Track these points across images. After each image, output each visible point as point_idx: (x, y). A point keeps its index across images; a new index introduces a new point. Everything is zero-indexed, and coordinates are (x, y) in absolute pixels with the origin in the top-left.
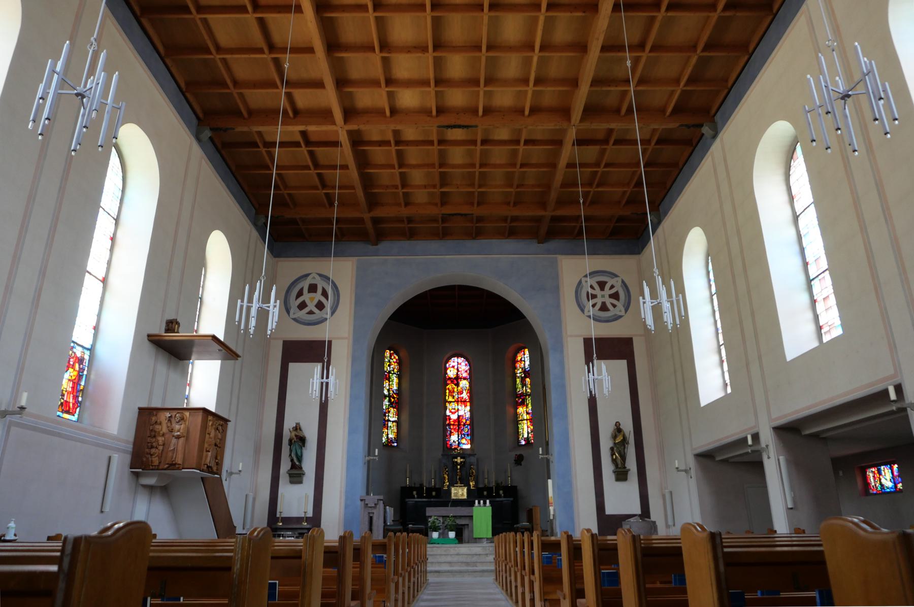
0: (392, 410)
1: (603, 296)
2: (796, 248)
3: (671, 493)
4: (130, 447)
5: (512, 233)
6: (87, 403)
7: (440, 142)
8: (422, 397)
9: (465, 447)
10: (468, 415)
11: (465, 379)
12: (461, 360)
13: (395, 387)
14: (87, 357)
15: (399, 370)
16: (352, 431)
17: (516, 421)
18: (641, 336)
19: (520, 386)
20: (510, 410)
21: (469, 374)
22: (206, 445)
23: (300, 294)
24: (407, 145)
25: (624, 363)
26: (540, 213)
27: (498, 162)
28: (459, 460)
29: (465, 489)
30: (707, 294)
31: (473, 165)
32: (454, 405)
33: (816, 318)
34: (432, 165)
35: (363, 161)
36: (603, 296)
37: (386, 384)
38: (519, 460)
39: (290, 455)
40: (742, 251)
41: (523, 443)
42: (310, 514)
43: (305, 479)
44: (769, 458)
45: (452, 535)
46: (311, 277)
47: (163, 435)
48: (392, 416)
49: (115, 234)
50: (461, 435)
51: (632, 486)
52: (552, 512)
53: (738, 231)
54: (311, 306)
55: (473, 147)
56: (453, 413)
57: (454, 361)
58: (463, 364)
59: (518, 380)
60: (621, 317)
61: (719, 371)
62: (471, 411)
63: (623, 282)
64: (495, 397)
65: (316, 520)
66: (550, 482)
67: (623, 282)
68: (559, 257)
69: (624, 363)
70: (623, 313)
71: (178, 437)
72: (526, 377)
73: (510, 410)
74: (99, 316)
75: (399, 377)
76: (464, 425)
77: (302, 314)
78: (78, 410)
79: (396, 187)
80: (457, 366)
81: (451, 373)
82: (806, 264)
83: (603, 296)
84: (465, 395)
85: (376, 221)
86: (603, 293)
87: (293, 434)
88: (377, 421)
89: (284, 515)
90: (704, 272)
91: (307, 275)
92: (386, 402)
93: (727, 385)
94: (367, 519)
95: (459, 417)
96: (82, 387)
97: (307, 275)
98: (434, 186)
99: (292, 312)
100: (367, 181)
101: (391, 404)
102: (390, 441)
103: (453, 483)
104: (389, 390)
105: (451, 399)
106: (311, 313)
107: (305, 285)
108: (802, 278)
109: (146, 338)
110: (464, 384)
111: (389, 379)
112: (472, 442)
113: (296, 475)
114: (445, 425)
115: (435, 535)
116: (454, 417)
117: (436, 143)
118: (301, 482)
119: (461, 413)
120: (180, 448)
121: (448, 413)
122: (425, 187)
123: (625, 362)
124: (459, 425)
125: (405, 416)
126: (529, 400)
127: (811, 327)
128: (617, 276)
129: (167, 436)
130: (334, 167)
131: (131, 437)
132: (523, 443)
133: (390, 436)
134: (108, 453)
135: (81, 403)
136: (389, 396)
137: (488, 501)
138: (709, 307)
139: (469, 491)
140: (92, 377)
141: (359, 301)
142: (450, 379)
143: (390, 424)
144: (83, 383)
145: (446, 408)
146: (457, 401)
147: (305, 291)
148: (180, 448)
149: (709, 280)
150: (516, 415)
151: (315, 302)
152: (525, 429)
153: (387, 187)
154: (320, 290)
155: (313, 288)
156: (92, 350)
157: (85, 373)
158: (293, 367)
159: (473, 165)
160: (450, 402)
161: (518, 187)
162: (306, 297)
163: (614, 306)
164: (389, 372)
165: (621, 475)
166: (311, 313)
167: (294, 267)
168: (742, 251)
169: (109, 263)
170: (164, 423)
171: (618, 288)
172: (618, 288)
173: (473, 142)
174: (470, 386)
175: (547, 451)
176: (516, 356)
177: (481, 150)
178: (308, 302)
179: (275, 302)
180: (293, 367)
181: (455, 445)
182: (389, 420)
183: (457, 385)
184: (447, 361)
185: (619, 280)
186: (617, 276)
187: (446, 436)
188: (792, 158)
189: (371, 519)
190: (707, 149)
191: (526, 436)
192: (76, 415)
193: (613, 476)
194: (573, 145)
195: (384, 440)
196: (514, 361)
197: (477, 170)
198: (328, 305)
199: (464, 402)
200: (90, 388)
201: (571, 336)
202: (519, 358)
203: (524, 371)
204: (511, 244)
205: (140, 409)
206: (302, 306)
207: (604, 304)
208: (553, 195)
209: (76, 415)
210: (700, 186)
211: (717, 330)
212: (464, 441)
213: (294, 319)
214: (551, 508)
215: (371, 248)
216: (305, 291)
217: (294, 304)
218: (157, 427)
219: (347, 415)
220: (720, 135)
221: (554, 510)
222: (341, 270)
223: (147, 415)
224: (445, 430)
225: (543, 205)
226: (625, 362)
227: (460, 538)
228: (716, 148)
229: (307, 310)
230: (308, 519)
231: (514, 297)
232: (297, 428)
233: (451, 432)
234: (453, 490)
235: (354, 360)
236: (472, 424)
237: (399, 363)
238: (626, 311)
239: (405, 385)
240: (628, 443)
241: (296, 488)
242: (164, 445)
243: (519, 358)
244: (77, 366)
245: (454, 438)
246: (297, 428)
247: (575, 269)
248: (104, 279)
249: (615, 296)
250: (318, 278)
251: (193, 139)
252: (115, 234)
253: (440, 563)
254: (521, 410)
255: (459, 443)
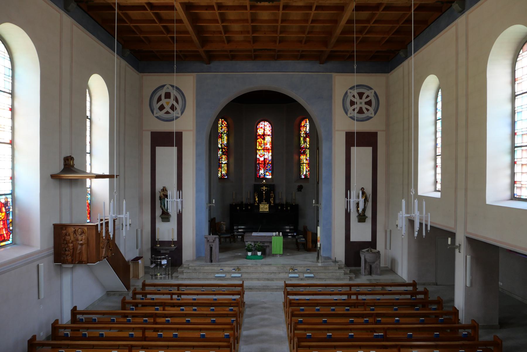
0: (224, 157)
1: (361, 103)
2: (509, 120)
3: (391, 231)
4: (52, 251)
5: (302, 56)
6: (17, 230)
7: (252, 7)
8: (243, 144)
9: (268, 177)
10: (270, 158)
11: (268, 135)
12: (266, 123)
13: (225, 142)
14: (10, 200)
15: (228, 131)
16: (198, 191)
17: (299, 163)
18: (383, 131)
19: (303, 142)
20: (296, 157)
21: (272, 133)
22: (101, 245)
23: (159, 99)
24: (227, 9)
25: (370, 149)
26: (323, 49)
27: (295, 19)
28: (264, 188)
29: (268, 205)
30: (433, 118)
31: (276, 21)
32: (262, 152)
33: (513, 174)
34: (246, 21)
35: (194, 19)
36: (360, 103)
37: (220, 141)
38: (300, 188)
39: (161, 206)
40: (467, 110)
41: (303, 177)
42: (176, 239)
43: (171, 219)
44: (460, 252)
45: (259, 253)
46: (165, 87)
47: (72, 243)
48: (224, 161)
49: (13, 105)
50: (266, 170)
51: (368, 226)
52: (319, 246)
53: (467, 95)
54: (167, 108)
55: (277, 12)
56: (261, 157)
57: (262, 124)
58: (268, 126)
59: (302, 139)
60: (371, 118)
61: (433, 172)
62: (272, 156)
63: (375, 93)
64: (286, 146)
65: (179, 243)
66: (319, 228)
67: (375, 93)
68: (334, 74)
69: (370, 149)
70: (373, 115)
71: (82, 245)
72: (306, 137)
73: (296, 157)
74: (13, 169)
75: (228, 136)
76: (268, 164)
77: (162, 113)
78: (11, 236)
79: (220, 32)
80: (265, 128)
81: (260, 132)
82: (514, 134)
83: (361, 103)
84: (269, 146)
85: (207, 52)
86: (361, 101)
87: (162, 194)
88: (213, 163)
89: (161, 239)
90: (432, 102)
91: (163, 86)
92: (220, 152)
93: (437, 182)
94: (209, 248)
95: (265, 159)
96: (11, 220)
97: (163, 86)
98: (248, 32)
99: (155, 112)
100: (199, 31)
101: (223, 153)
102: (222, 175)
103: (260, 201)
104: (221, 145)
105: (260, 148)
106: (167, 113)
107: (163, 93)
108: (508, 144)
109: (50, 177)
110: (268, 139)
111: (221, 137)
112: (272, 174)
113: (166, 217)
114: (256, 164)
115: (250, 254)
116: (262, 159)
117: (248, 8)
118: (169, 221)
119: (266, 157)
120: (84, 252)
121: (258, 156)
122: (242, 32)
123: (371, 148)
124: (265, 164)
125: (232, 160)
126: (308, 151)
127: (507, 181)
128: (371, 89)
129: (74, 243)
130: (172, 21)
131: (52, 244)
132: (303, 177)
133: (223, 173)
134: (35, 264)
135: (12, 230)
136: (222, 148)
137: (281, 233)
138: (433, 129)
139: (270, 207)
140: (17, 212)
141: (198, 105)
142: (259, 135)
143: (223, 165)
144: (11, 217)
145: (257, 154)
146: (264, 149)
147: (163, 97)
148: (84, 252)
149: (436, 109)
150: (300, 160)
151: (170, 105)
152: (305, 170)
153: (214, 32)
154: (172, 97)
155: (168, 95)
156: (12, 194)
157: (11, 210)
158: (159, 149)
159: (276, 21)
160: (260, 150)
161: (309, 33)
162: (164, 101)
163: (368, 110)
164: (222, 133)
165: (362, 218)
166: (167, 113)
167: (153, 80)
168: (467, 110)
169: (13, 128)
170: (72, 234)
171: (372, 98)
172: (372, 98)
173: (277, 8)
174: (272, 140)
175: (317, 202)
176: (301, 123)
177: (283, 13)
178: (165, 105)
179: (126, 213)
180: (159, 149)
181: (262, 176)
182: (222, 163)
183: (264, 139)
184: (258, 124)
185: (373, 91)
186: (371, 89)
187: (257, 171)
188: (522, 48)
189: (211, 248)
190: (453, 19)
191: (305, 173)
192: (11, 240)
193: (357, 219)
194: (353, 10)
195: (219, 175)
196: (300, 126)
197: (279, 24)
198: (179, 107)
199: (268, 150)
200: (17, 219)
201: (338, 131)
202: (303, 124)
203: (306, 133)
204: (301, 64)
205: (54, 225)
206: (162, 108)
207: (361, 109)
208: (333, 40)
209: (11, 240)
210: (443, 43)
211: (436, 145)
212: (267, 174)
213: (157, 117)
214: (319, 244)
215: (206, 66)
216: (163, 97)
217: (156, 106)
218: (68, 238)
219: (195, 181)
220: (467, 13)
221: (320, 245)
222: (187, 82)
223: (59, 231)
224: (256, 167)
225: (325, 43)
226: (371, 148)
227: (264, 254)
228: (461, 20)
229: (164, 111)
230: (174, 242)
231: (301, 100)
232: (164, 190)
233: (260, 168)
234: (261, 206)
235: (197, 145)
236: (272, 164)
237: (228, 126)
238: (375, 113)
239: (232, 141)
240: (368, 201)
241: (166, 225)
242: (73, 248)
243: (303, 124)
244: (4, 209)
245: (262, 172)
246: (164, 190)
247: (343, 83)
248: (11, 141)
249: (369, 103)
250: (171, 88)
251: (62, 12)
252: (13, 105)
253: (252, 279)
254: (303, 157)
255: (265, 175)
